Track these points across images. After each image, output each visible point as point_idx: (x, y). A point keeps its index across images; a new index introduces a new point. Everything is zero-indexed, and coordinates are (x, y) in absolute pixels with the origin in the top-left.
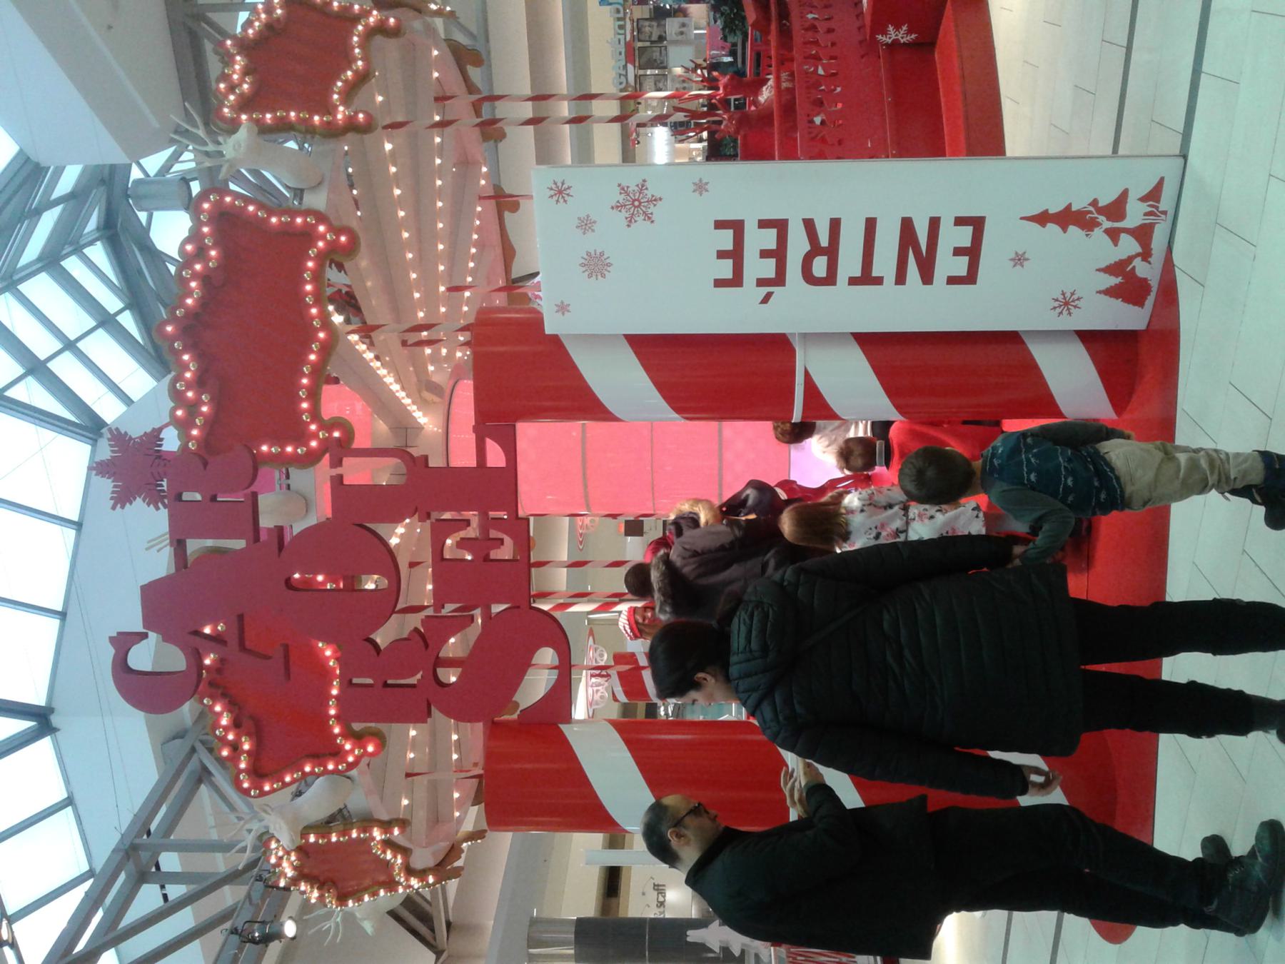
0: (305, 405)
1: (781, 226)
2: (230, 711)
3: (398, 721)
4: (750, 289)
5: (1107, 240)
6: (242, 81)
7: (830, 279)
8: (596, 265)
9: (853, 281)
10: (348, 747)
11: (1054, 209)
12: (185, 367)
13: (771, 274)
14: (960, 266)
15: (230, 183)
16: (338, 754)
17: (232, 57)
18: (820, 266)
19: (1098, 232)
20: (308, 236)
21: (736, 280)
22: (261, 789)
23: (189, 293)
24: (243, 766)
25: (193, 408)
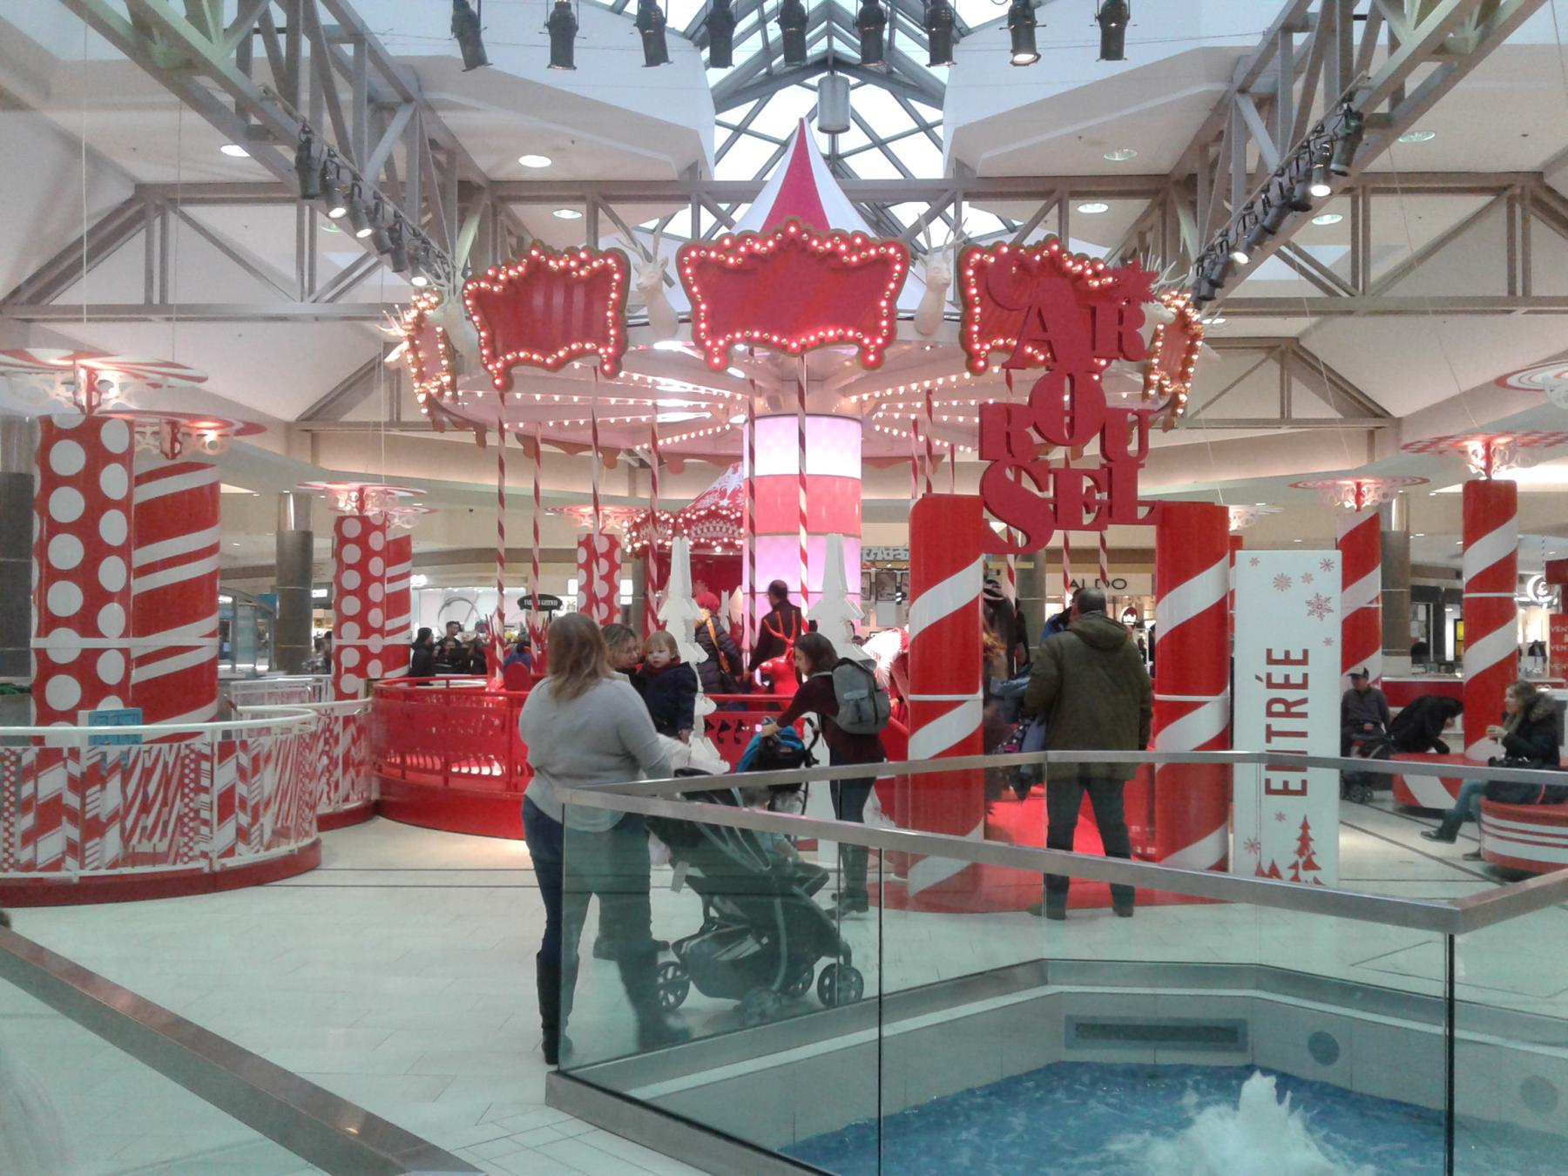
0: (812, 338)
1: (1304, 686)
2: (519, 277)
4: (1264, 669)
5: (1292, 862)
7: (1270, 714)
8: (1282, 582)
9: (1268, 727)
10: (499, 365)
11: (1311, 833)
12: (764, 244)
13: (1274, 681)
14: (1277, 784)
15: (600, 210)
16: (494, 357)
19: (1296, 857)
20: (874, 331)
21: (1271, 661)
22: (468, 298)
23: (822, 243)
24: (595, 264)
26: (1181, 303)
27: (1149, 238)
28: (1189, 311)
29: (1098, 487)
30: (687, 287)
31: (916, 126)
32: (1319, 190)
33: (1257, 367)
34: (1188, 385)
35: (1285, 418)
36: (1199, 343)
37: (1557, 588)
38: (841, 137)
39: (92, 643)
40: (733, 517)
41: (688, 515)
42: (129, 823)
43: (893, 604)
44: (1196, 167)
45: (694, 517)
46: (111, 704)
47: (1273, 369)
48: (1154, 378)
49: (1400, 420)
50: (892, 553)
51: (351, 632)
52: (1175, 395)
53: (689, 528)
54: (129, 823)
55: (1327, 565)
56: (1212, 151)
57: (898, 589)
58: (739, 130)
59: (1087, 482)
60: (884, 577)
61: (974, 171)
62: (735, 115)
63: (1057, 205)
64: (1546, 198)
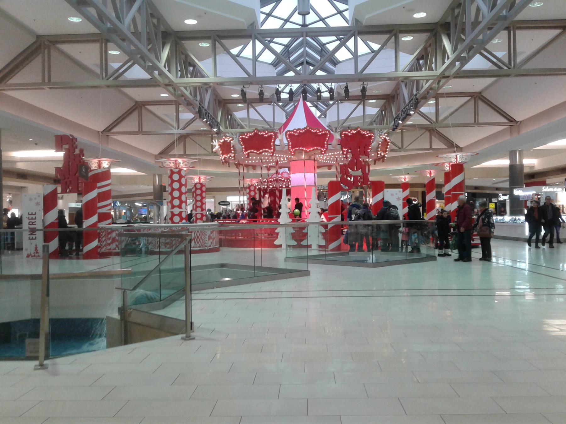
1: (35, 219)
3: (510, 157)
6: (351, 133)
7: (29, 224)
8: (392, 195)
15: (47, 49)
16: (246, 151)
17: (356, 130)
18: (31, 223)
20: (323, 147)
21: (29, 214)
25: (296, 132)
26: (384, 137)
27: (429, 49)
28: (387, 138)
29: (361, 178)
30: (287, 139)
31: (336, 12)
32: (412, 113)
33: (424, 133)
34: (387, 153)
35: (431, 148)
36: (389, 144)
37: (272, 196)
38: (307, 16)
39: (172, 210)
40: (282, 180)
41: (271, 180)
42: (195, 240)
43: (323, 202)
44: (449, 19)
45: (272, 180)
46: (184, 221)
47: (428, 134)
48: (379, 153)
49: (462, 148)
50: (323, 187)
51: (199, 210)
52: (384, 155)
53: (271, 183)
54: (195, 240)
55: (400, 192)
56: (457, 11)
57: (325, 197)
58: (269, 15)
59: (359, 178)
60: (321, 194)
61: (362, 23)
62: (267, 9)
63: (394, 36)
64: (481, 97)
